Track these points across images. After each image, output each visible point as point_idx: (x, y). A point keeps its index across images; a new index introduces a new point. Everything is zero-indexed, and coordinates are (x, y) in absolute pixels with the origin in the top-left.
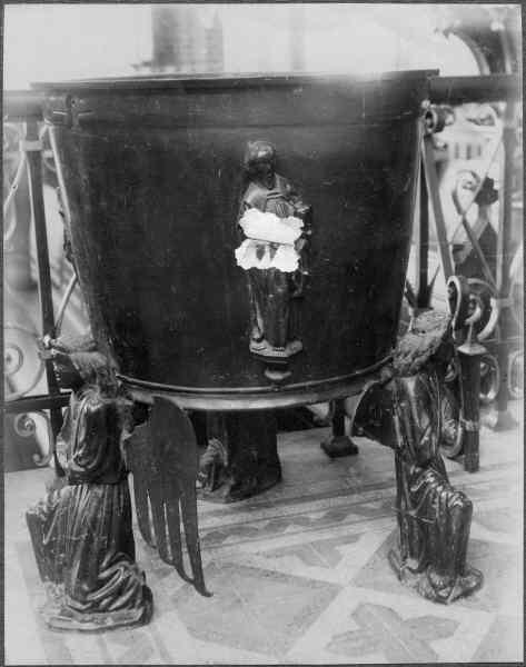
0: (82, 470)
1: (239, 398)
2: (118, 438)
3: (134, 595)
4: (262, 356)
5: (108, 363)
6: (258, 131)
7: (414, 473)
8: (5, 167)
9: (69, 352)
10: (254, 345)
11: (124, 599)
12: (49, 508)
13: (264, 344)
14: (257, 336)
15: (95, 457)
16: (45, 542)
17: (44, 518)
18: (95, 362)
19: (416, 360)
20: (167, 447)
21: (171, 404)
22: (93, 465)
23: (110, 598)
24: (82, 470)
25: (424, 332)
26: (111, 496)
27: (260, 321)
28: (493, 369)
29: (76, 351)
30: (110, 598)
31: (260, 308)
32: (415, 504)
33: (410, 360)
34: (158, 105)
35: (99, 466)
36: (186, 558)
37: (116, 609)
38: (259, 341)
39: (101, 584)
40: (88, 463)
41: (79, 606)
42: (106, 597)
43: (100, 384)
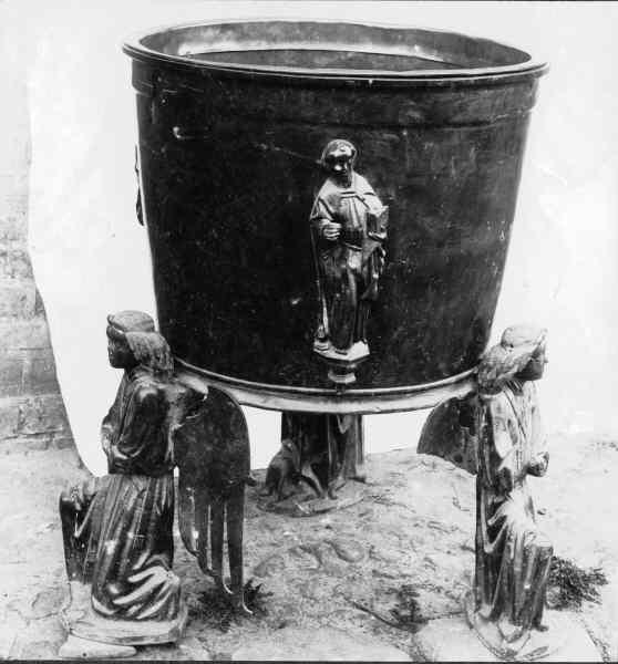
0: (125, 457)
1: (299, 399)
2: (167, 429)
3: (167, 606)
4: (323, 357)
5: (165, 347)
6: (340, 130)
7: (493, 503)
8: (218, 659)
9: (127, 331)
10: (317, 343)
11: (159, 605)
12: (85, 496)
13: (327, 344)
14: (321, 336)
15: (139, 446)
16: (77, 534)
17: (78, 507)
18: (151, 343)
19: (500, 377)
20: (384, 178)
21: (227, 397)
22: (136, 454)
23: (140, 606)
24: (125, 457)
25: (512, 346)
26: (152, 489)
27: (325, 319)
28: (339, 465)
29: (132, 330)
30: (140, 606)
31: (327, 302)
32: (492, 537)
33: (494, 376)
34: (234, 96)
35: (143, 455)
36: (226, 564)
37: (146, 619)
38: (323, 340)
39: (129, 588)
40: (133, 452)
41: (104, 609)
42: (134, 603)
43: (155, 368)
